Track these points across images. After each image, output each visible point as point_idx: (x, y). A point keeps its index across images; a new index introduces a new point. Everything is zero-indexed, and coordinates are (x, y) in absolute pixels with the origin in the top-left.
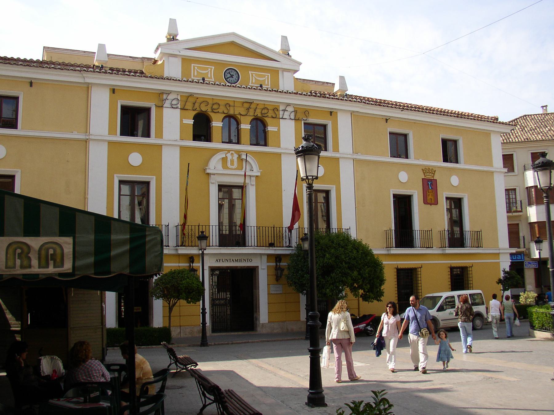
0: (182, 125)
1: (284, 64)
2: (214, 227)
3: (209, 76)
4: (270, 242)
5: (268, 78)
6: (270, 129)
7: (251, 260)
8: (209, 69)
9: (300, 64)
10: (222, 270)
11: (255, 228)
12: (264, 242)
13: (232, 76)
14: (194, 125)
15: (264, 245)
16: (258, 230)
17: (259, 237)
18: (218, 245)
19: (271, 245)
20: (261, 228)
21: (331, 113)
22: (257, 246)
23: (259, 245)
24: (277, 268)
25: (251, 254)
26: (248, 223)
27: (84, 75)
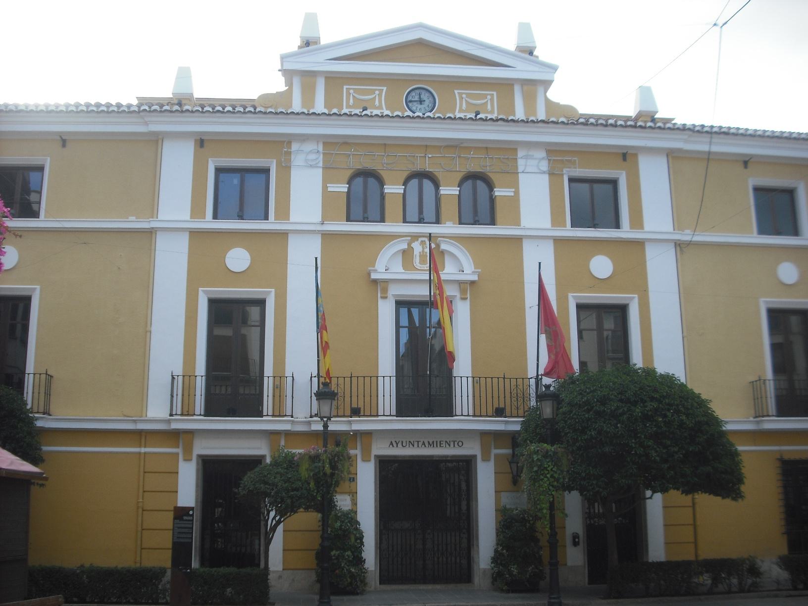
0: (327, 198)
1: (522, 71)
2: (387, 379)
3: (377, 103)
4: (354, 406)
5: (380, 95)
6: (498, 192)
7: (460, 444)
8: (377, 92)
9: (554, 68)
11: (470, 379)
12: (484, 406)
13: (421, 102)
15: (484, 413)
16: (477, 386)
17: (36, 395)
18: (394, 412)
19: (499, 412)
20: (483, 381)
21: (624, 156)
22: (474, 416)
23: (478, 413)
24: (513, 460)
27: (147, 119)
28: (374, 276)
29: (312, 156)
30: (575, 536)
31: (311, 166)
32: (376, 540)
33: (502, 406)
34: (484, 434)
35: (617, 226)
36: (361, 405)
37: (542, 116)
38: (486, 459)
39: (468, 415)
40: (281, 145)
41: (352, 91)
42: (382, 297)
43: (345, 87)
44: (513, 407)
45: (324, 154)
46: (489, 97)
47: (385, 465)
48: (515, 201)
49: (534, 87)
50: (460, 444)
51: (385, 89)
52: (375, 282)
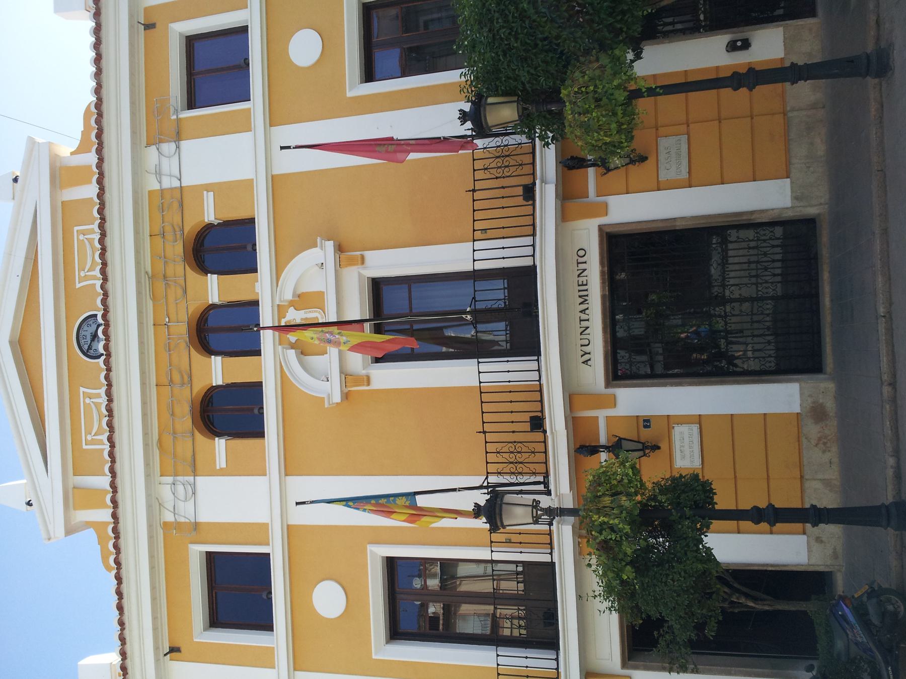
0: (234, 469)
4: (527, 427)
6: (210, 216)
7: (582, 252)
8: (88, 401)
9: (31, 142)
10: (616, 346)
11: (479, 245)
14: (220, 273)
15: (528, 220)
19: (529, 192)
22: (534, 235)
25: (565, 261)
26: (467, 266)
28: (337, 398)
29: (180, 489)
30: (732, 47)
31: (194, 493)
32: (738, 383)
33: (520, 191)
34: (563, 216)
35: (243, 30)
36: (526, 417)
37: (91, 158)
38: (604, 210)
39: (533, 246)
40: (173, 534)
41: (89, 438)
42: (368, 384)
43: (85, 447)
44: (519, 172)
45: (176, 475)
46: (81, 237)
47: (618, 374)
48: (221, 190)
49: (61, 175)
50: (581, 253)
51: (82, 389)
52: (346, 396)
